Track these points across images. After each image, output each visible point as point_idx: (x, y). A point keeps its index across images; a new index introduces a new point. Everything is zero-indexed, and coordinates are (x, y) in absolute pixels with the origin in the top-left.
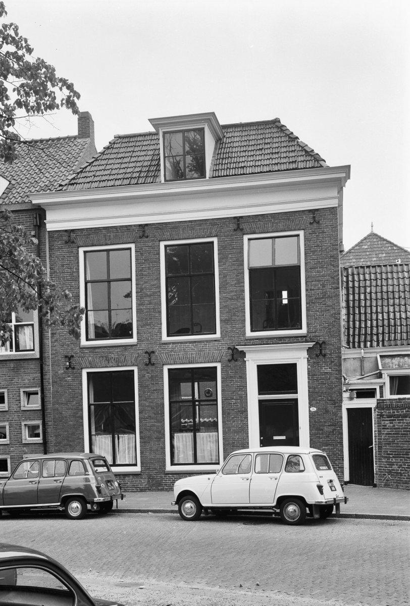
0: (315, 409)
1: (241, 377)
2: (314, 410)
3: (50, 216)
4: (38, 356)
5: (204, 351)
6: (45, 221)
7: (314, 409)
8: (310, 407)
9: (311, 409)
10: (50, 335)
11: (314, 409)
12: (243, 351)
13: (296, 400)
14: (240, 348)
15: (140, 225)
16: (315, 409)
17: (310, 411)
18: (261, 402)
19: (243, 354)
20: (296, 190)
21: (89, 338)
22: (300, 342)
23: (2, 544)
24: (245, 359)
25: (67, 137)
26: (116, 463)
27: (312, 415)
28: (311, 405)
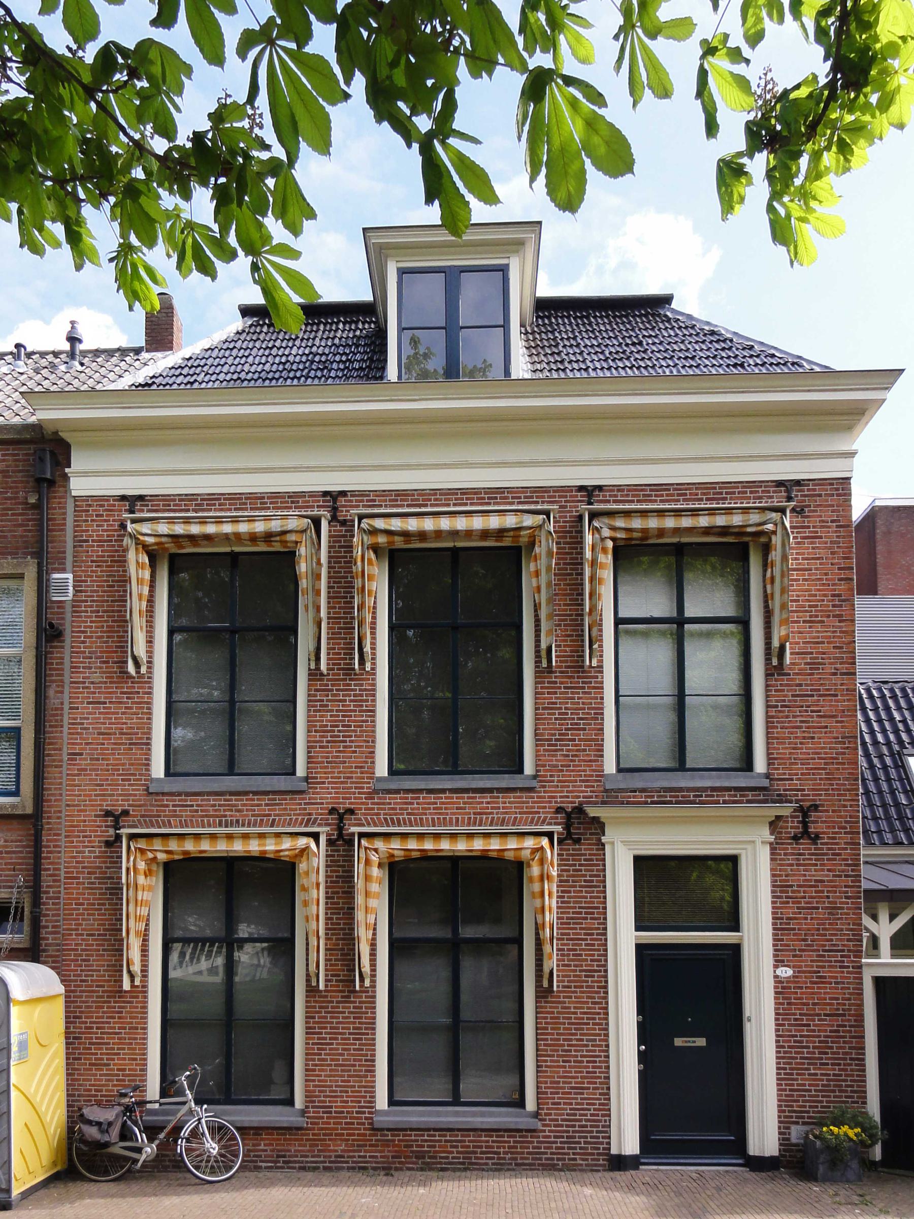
0: (789, 972)
1: (589, 885)
2: (784, 975)
3: (79, 462)
4: (29, 810)
5: (492, 813)
6: (67, 470)
7: (786, 972)
8: (776, 967)
9: (778, 972)
10: (65, 758)
11: (786, 972)
12: (598, 818)
13: (736, 950)
14: (592, 812)
15: (326, 494)
16: (789, 972)
17: (776, 977)
18: (641, 949)
19: (598, 825)
20: (57, 1156)
21: (172, 771)
22: (749, 802)
23: (875, 9)
24: (604, 839)
25: (119, 349)
26: (687, 766)
27: (782, 989)
28: (779, 962)
